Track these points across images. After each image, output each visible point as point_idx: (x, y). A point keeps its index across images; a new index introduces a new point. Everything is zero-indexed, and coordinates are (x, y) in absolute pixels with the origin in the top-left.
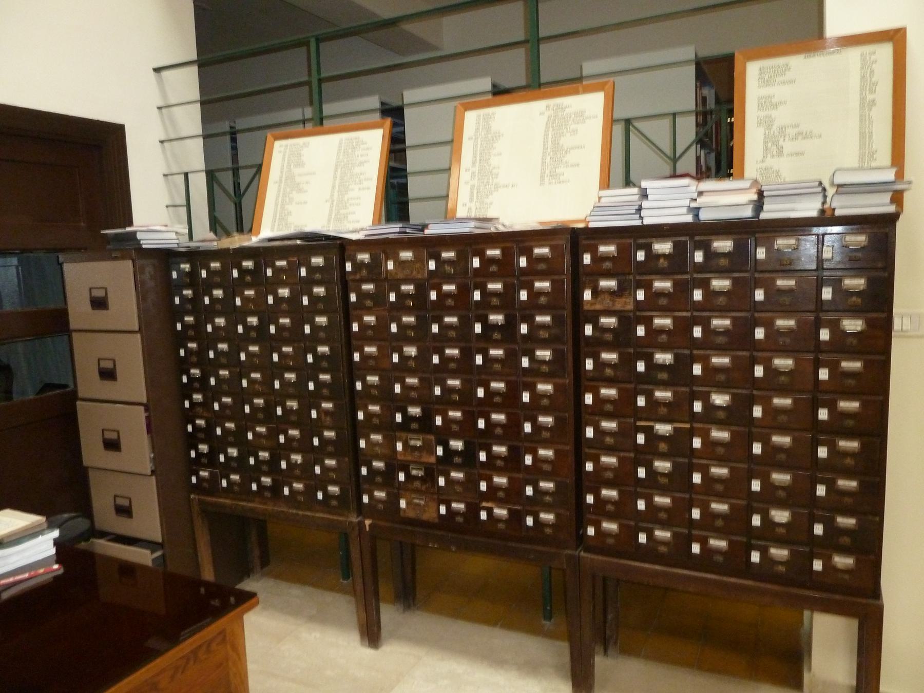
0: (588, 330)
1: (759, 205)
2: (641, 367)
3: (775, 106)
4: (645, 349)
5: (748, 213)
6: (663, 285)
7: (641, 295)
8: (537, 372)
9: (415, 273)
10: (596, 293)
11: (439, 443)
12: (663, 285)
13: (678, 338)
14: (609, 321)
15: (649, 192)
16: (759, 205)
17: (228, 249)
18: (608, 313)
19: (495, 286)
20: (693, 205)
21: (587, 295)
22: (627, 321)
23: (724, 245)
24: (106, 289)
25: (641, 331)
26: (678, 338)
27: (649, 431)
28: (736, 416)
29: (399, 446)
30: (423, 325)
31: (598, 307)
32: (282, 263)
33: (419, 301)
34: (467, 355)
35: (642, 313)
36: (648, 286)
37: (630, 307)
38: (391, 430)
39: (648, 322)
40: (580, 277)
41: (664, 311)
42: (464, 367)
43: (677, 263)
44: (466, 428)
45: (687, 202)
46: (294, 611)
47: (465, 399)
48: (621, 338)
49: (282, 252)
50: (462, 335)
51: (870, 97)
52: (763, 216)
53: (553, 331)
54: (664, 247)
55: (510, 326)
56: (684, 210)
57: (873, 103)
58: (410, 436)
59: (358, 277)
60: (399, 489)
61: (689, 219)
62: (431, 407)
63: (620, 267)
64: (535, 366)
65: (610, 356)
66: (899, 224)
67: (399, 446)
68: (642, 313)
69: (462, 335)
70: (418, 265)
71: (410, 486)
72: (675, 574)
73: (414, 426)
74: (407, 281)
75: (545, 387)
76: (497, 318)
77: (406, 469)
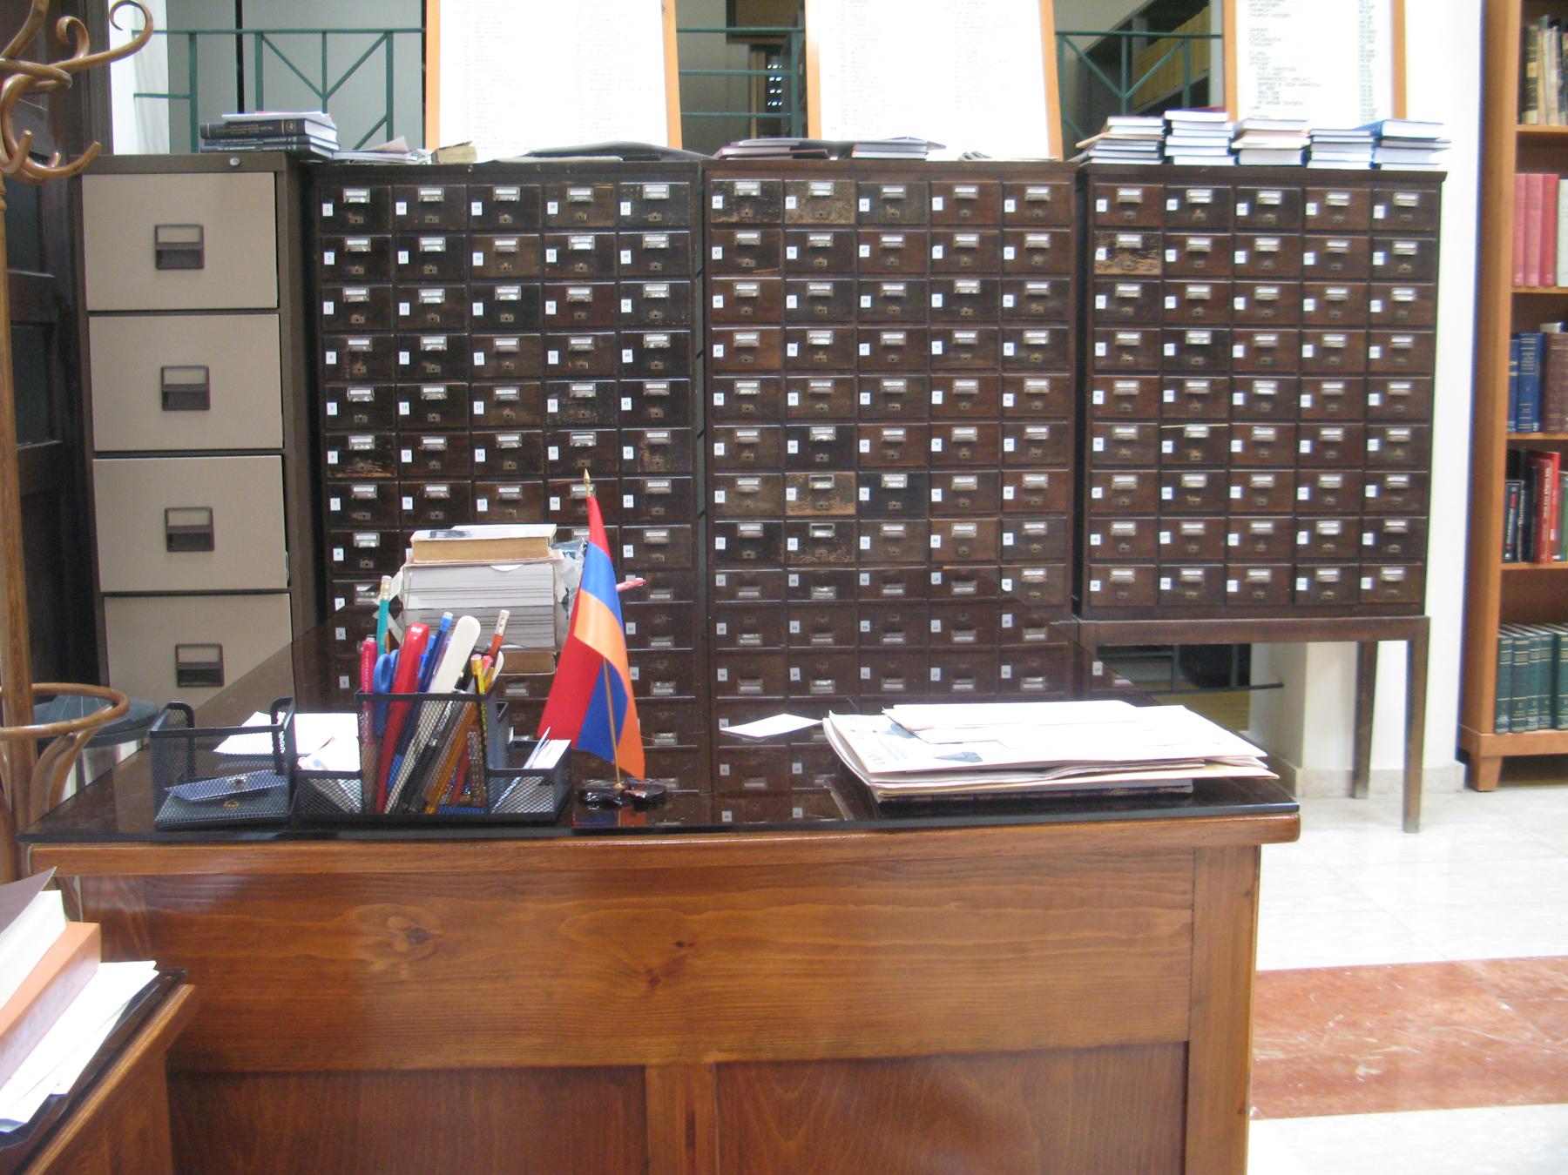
0: (1101, 302)
1: (1306, 153)
2: (1169, 350)
3: (1269, 42)
4: (1173, 327)
5: (1296, 160)
6: (1199, 243)
7: (1171, 255)
8: (1026, 363)
9: (833, 216)
10: (1113, 252)
11: (862, 482)
12: (1199, 243)
14: (1130, 290)
15: (1174, 125)
16: (1306, 153)
17: (466, 166)
18: (1128, 279)
19: (967, 239)
20: (1235, 145)
21: (1101, 254)
22: (1154, 291)
23: (1271, 197)
24: (201, 228)
25: (1170, 303)
27: (1178, 436)
28: (1281, 409)
29: (791, 494)
30: (845, 295)
31: (1115, 271)
32: (581, 194)
33: (840, 258)
34: (919, 341)
35: (1169, 280)
36: (1180, 244)
37: (1157, 271)
38: (774, 466)
39: (1179, 291)
40: (1087, 231)
41: (1200, 276)
42: (912, 359)
43: (526, 214)
44: (911, 455)
45: (1225, 143)
46: (1479, 746)
47: (912, 409)
48: (1145, 312)
49: (583, 174)
50: (912, 312)
51: (1369, 47)
52: (1311, 165)
53: (1052, 304)
54: (1201, 195)
55: (989, 294)
56: (1224, 152)
57: (1371, 54)
58: (812, 475)
59: (735, 219)
60: (786, 564)
61: (1230, 162)
62: (851, 424)
63: (1289, 219)
64: (1023, 354)
65: (1129, 337)
66: (1444, 184)
67: (791, 494)
68: (1169, 280)
69: (912, 312)
70: (840, 204)
71: (808, 558)
72: (605, 697)
73: (822, 457)
74: (820, 227)
75: (1037, 384)
76: (968, 286)
77: (801, 531)
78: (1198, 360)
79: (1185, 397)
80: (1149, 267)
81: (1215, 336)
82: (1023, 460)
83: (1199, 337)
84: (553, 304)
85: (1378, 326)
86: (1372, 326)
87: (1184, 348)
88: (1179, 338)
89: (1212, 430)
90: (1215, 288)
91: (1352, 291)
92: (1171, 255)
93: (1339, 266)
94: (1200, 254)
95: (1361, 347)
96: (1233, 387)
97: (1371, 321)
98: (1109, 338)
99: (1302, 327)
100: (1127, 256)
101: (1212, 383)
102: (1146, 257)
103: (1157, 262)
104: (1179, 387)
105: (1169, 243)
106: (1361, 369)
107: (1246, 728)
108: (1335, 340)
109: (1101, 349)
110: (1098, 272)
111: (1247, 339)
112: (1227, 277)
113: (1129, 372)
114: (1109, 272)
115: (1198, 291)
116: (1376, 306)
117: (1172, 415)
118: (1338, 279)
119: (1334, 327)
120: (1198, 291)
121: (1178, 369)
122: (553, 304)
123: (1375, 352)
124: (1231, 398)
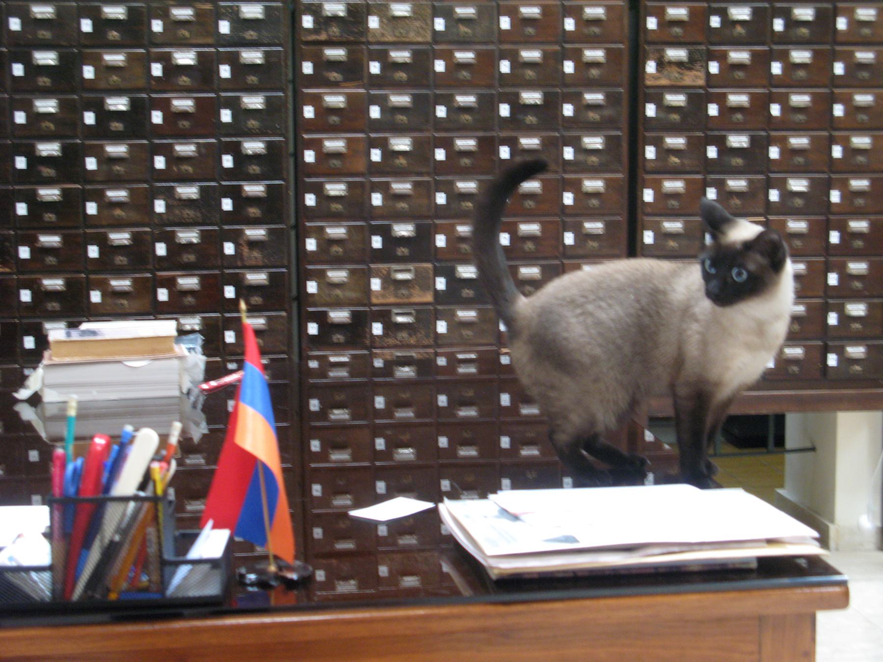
0: (651, 110)
7: (714, 68)
10: (662, 64)
13: (754, 118)
14: (677, 99)
18: (675, 89)
21: (651, 67)
26: (754, 118)
31: (664, 82)
37: (701, 82)
39: (721, 100)
48: (691, 119)
78: (738, 161)
80: (693, 78)
88: (720, 142)
94: (740, 66)
96: (769, 184)
98: (658, 143)
103: (702, 74)
105: (712, 56)
113: (674, 172)
115: (738, 99)
120: (738, 99)
124: (767, 195)
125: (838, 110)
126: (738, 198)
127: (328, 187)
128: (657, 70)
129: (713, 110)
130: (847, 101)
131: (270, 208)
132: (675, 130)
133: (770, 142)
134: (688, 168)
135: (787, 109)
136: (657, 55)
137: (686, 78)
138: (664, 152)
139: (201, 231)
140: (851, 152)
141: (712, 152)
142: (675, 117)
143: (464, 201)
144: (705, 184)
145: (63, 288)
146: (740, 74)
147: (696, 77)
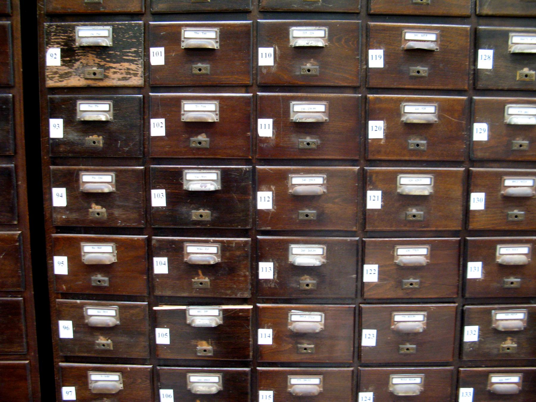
0: (56, 128)
2: (159, 198)
7: (157, 56)
10: (70, 53)
18: (93, 92)
21: (53, 57)
31: (75, 81)
36: (171, 39)
37: (137, 81)
39: (171, 111)
78: (203, 214)
79: (185, 269)
80: (125, 74)
81: (226, 178)
82: (286, 78)
83: (201, 180)
84: (269, 122)
85: (482, 162)
86: (474, 162)
87: (179, 196)
88: (173, 182)
89: (227, 315)
90: (225, 106)
91: (443, 110)
92: (157, 56)
93: (423, 70)
94: (199, 53)
95: (458, 191)
96: (259, 253)
97: (471, 155)
98: (71, 182)
99: (365, 163)
100: (92, 58)
101: (225, 248)
102: (120, 61)
103: (137, 67)
104: (175, 253)
105: (152, 38)
106: (456, 226)
107: (260, 387)
108: (416, 183)
109: (59, 197)
110: (50, 83)
111: (279, 182)
112: (246, 88)
113: (101, 230)
114: (64, 83)
115: (200, 109)
116: (481, 132)
117: (169, 293)
118: (420, 90)
119: (416, 162)
120: (200, 109)
121: (176, 224)
122: (269, 122)
123: (478, 201)
124: (255, 271)
125: (376, 130)
126: (205, 274)
127: (191, 249)
128: (64, 62)
129: (158, 128)
130: (391, 114)
131: (223, 280)
132: (98, 160)
133: (258, 182)
134: (119, 224)
135: (286, 126)
136: (63, 37)
137: (110, 73)
138: (81, 198)
139: (225, 311)
140: (397, 201)
141: (159, 198)
142: (96, 140)
143: (508, 276)
144: (151, 252)
145: (121, 386)
146: (203, 67)
147: (128, 71)
